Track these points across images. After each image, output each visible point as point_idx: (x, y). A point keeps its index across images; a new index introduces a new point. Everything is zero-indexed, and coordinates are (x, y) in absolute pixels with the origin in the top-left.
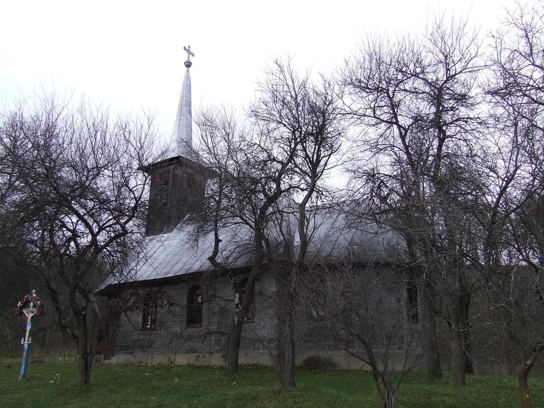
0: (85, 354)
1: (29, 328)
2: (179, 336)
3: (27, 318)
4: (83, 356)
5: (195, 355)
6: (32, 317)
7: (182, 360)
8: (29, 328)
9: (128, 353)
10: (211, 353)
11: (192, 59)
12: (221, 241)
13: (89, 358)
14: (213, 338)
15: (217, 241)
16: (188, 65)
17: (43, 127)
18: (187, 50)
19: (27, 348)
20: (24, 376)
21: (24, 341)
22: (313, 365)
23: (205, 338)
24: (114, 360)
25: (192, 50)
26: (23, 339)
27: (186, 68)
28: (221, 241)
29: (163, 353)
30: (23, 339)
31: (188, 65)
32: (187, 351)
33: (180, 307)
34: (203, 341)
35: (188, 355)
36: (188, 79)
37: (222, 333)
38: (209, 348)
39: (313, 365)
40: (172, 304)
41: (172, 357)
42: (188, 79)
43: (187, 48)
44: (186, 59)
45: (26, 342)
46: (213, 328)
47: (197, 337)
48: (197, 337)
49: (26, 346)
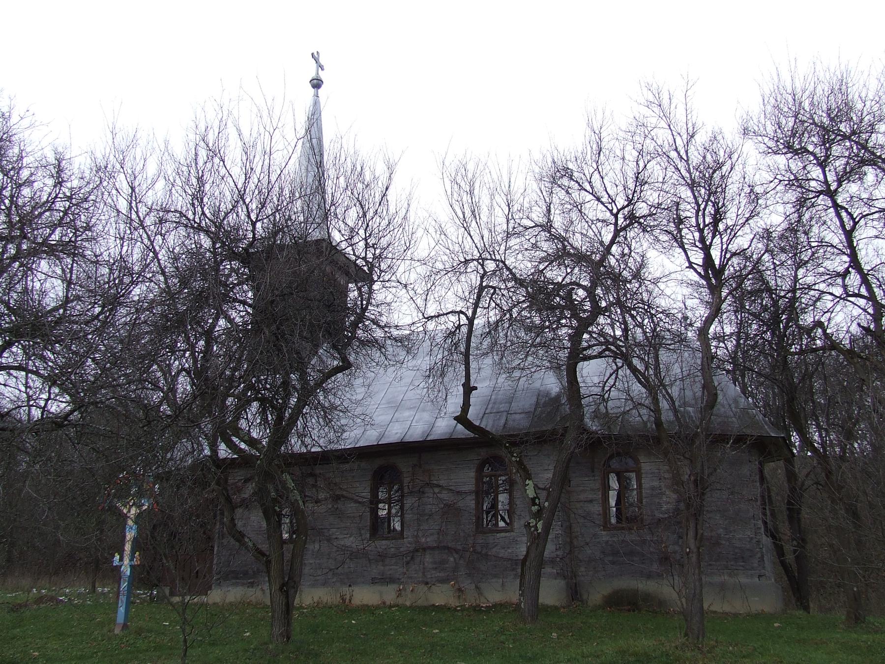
0: (283, 585)
1: (130, 535)
2: (355, 555)
3: (126, 517)
4: (281, 589)
5: (395, 587)
6: (138, 517)
7: (364, 595)
8: (130, 535)
9: (243, 584)
10: (427, 583)
11: (323, 75)
12: (475, 388)
13: (292, 591)
14: (428, 558)
15: (468, 389)
16: (317, 84)
17: (781, 160)
18: (315, 57)
19: (128, 573)
20: (125, 626)
21: (121, 559)
22: (624, 603)
23: (412, 558)
24: (215, 596)
25: (322, 61)
26: (117, 557)
27: (312, 91)
28: (475, 388)
29: (325, 584)
30: (117, 557)
31: (317, 84)
32: (374, 581)
33: (356, 502)
34: (408, 563)
35: (378, 588)
36: (316, 103)
37: (448, 548)
38: (421, 575)
39: (624, 603)
40: (337, 498)
41: (345, 590)
42: (316, 103)
43: (315, 54)
44: (313, 75)
45: (126, 561)
46: (431, 541)
47: (394, 556)
48: (394, 556)
49: (126, 570)
